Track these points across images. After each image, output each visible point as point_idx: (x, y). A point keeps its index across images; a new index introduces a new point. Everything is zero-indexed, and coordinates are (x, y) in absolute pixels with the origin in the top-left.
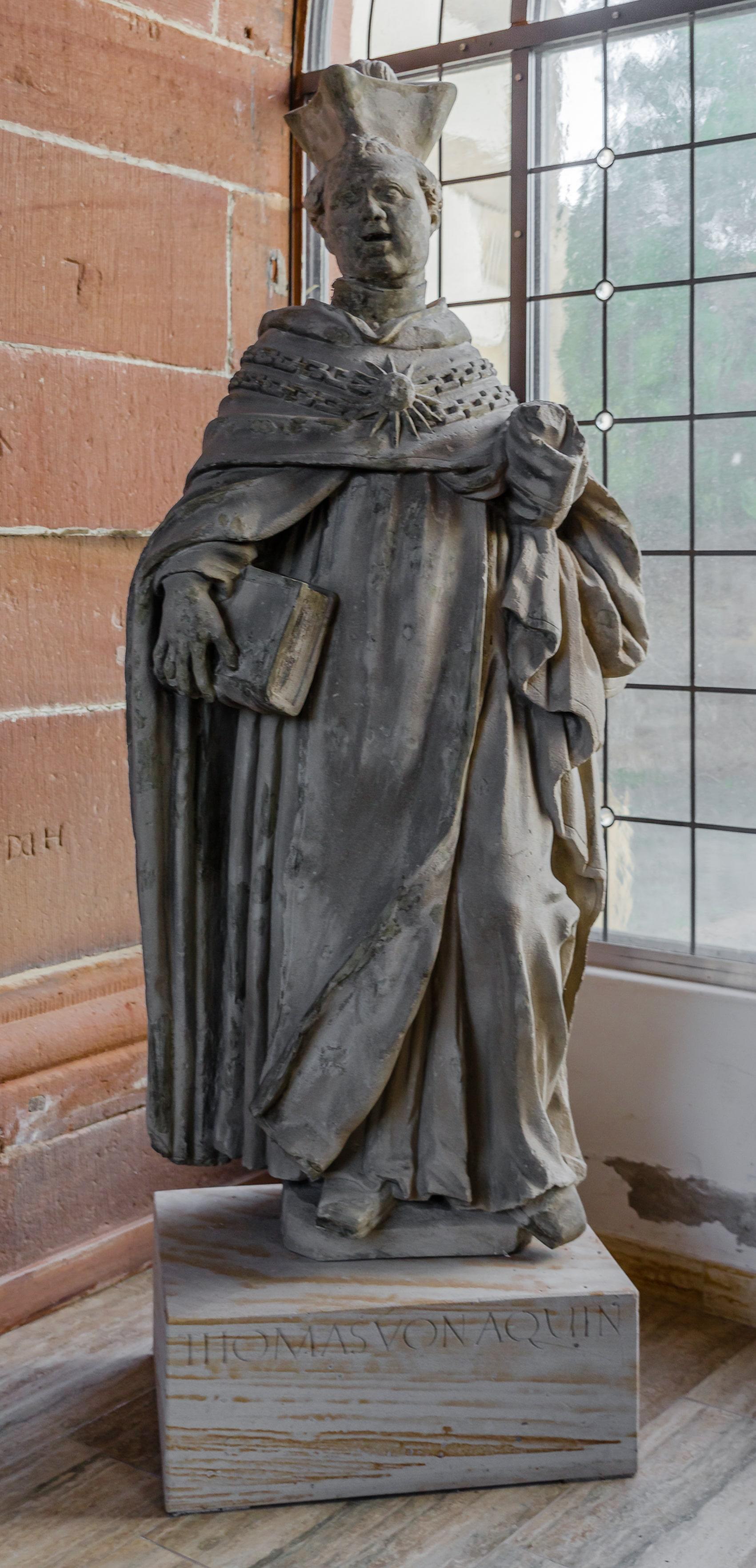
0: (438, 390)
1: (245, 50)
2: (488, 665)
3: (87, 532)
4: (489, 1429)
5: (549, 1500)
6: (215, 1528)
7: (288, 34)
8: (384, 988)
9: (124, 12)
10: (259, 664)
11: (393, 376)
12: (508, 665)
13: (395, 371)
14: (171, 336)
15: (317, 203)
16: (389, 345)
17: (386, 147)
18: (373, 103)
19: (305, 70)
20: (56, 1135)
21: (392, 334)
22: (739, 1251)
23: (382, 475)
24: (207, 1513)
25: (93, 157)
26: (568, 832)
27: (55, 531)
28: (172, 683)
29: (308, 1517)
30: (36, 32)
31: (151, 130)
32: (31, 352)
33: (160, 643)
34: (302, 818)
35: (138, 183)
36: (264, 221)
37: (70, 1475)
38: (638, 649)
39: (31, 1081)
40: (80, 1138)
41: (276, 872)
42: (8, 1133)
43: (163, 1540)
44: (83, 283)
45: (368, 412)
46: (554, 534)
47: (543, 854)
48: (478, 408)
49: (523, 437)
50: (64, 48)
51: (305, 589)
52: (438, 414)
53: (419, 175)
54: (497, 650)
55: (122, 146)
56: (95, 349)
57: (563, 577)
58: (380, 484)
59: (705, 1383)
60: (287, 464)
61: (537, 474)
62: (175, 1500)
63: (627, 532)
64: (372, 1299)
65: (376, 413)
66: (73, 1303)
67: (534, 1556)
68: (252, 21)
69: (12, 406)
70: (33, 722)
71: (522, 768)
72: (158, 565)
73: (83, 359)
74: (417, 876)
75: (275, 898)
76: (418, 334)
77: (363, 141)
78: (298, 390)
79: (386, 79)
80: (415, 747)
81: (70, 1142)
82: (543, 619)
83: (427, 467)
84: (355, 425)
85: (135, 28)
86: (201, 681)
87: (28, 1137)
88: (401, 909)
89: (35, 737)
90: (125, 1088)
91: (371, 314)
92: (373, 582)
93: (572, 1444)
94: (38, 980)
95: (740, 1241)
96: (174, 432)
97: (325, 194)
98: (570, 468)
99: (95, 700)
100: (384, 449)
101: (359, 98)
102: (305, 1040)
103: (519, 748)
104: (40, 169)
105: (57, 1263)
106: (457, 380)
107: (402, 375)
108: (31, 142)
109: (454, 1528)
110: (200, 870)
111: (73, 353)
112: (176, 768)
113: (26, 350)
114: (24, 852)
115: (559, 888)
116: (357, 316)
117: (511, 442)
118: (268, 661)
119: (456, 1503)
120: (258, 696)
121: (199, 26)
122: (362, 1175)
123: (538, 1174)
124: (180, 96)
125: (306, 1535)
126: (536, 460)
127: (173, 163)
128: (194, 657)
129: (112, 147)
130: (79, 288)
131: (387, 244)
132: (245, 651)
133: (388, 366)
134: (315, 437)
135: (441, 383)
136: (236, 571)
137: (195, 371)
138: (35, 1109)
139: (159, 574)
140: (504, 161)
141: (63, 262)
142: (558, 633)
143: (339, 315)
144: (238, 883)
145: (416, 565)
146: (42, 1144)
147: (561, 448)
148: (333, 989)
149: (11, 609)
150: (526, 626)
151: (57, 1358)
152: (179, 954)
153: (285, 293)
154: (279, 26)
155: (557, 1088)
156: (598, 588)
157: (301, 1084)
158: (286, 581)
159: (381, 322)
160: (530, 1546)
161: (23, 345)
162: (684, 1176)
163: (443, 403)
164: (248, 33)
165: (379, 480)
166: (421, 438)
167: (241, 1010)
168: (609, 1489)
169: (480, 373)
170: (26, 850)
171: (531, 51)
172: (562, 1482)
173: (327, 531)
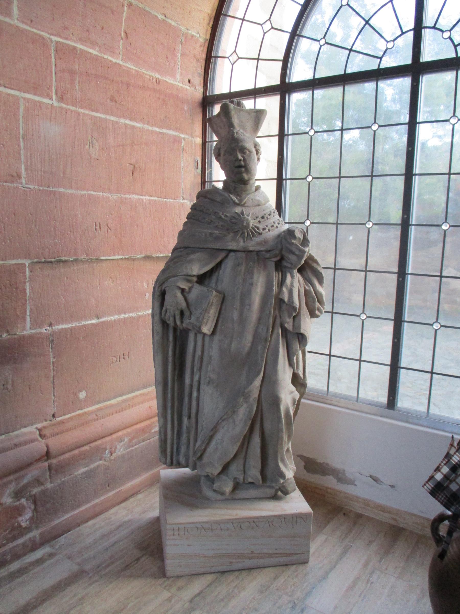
0: (259, 222)
1: (188, 88)
2: (274, 317)
3: (136, 256)
4: (266, 551)
5: (283, 572)
6: (180, 583)
7: (202, 81)
8: (237, 423)
9: (148, 75)
10: (198, 318)
11: (245, 218)
12: (280, 317)
13: (245, 216)
14: (163, 188)
15: (218, 152)
16: (243, 205)
17: (243, 134)
18: (238, 116)
19: (208, 95)
20: (128, 449)
21: (244, 202)
22: (337, 484)
23: (240, 253)
24: (178, 577)
25: (137, 127)
26: (298, 371)
27: (125, 257)
28: (168, 322)
29: (210, 578)
30: (118, 83)
31: (157, 117)
32: (117, 197)
33: (164, 309)
34: (211, 367)
35: (153, 136)
36: (194, 148)
37: (136, 562)
38: (322, 310)
39: (120, 433)
40: (136, 449)
41: (202, 382)
42: (113, 450)
43: (166, 586)
44: (134, 172)
45: (235, 230)
46: (297, 271)
47: (290, 379)
48: (273, 228)
49: (289, 240)
50: (127, 88)
51: (214, 293)
52: (260, 231)
53: (254, 144)
54: (277, 312)
55: (147, 123)
56: (138, 195)
57: (299, 287)
58: (239, 255)
59: (327, 527)
60: (208, 248)
61: (293, 253)
62: (168, 574)
63: (320, 271)
64: (231, 515)
65: (239, 231)
66: (134, 497)
67: (280, 593)
68: (190, 77)
69: (111, 216)
70: (119, 320)
71: (284, 352)
72: (164, 283)
73: (134, 198)
74: (249, 388)
75: (201, 391)
76: (253, 201)
77: (235, 131)
78: (211, 221)
79: (242, 107)
80: (249, 345)
81: (132, 450)
82: (293, 302)
83: (256, 250)
84: (231, 234)
85: (151, 81)
86: (178, 323)
87: (119, 451)
88: (243, 399)
89: (120, 325)
90: (149, 432)
91: (236, 194)
92: (237, 290)
93: (290, 555)
94: (122, 401)
95: (338, 482)
96: (164, 221)
97: (221, 149)
98: (305, 252)
99: (139, 311)
100: (241, 244)
101: (234, 115)
102: (211, 438)
103: (283, 344)
104: (119, 132)
105: (128, 486)
106: (266, 218)
107: (248, 217)
108: (116, 122)
109: (254, 583)
110: (176, 378)
111: (131, 196)
112: (169, 347)
113: (115, 196)
114: (117, 361)
115: (293, 388)
116: (232, 194)
117: (284, 242)
118: (201, 317)
119: (255, 572)
120: (198, 329)
121: (173, 79)
122: (227, 476)
123: (282, 475)
124: (166, 105)
125: (209, 585)
126: (293, 249)
127: (164, 128)
128: (176, 315)
129: (144, 123)
130: (133, 173)
131: (243, 169)
132: (193, 313)
133: (242, 213)
134: (218, 238)
135: (261, 219)
136: (190, 285)
137: (171, 200)
138: (121, 442)
139: (163, 287)
140: (276, 132)
141: (127, 165)
142: (298, 307)
143: (226, 194)
144: (189, 383)
145: (251, 284)
146: (124, 452)
147: (301, 245)
148: (220, 423)
149: (112, 284)
150: (287, 304)
151: (130, 517)
152: (169, 404)
153: (200, 172)
154: (199, 79)
155: (289, 446)
156: (310, 290)
157: (209, 450)
158: (208, 290)
159: (240, 197)
160: (278, 589)
161: (114, 194)
162: (322, 462)
163: (261, 227)
164: (189, 81)
165: (239, 254)
166: (254, 239)
167: (189, 423)
168: (301, 568)
169: (273, 215)
170: (117, 361)
171: (287, 92)
172: (286, 565)
173: (221, 271)
